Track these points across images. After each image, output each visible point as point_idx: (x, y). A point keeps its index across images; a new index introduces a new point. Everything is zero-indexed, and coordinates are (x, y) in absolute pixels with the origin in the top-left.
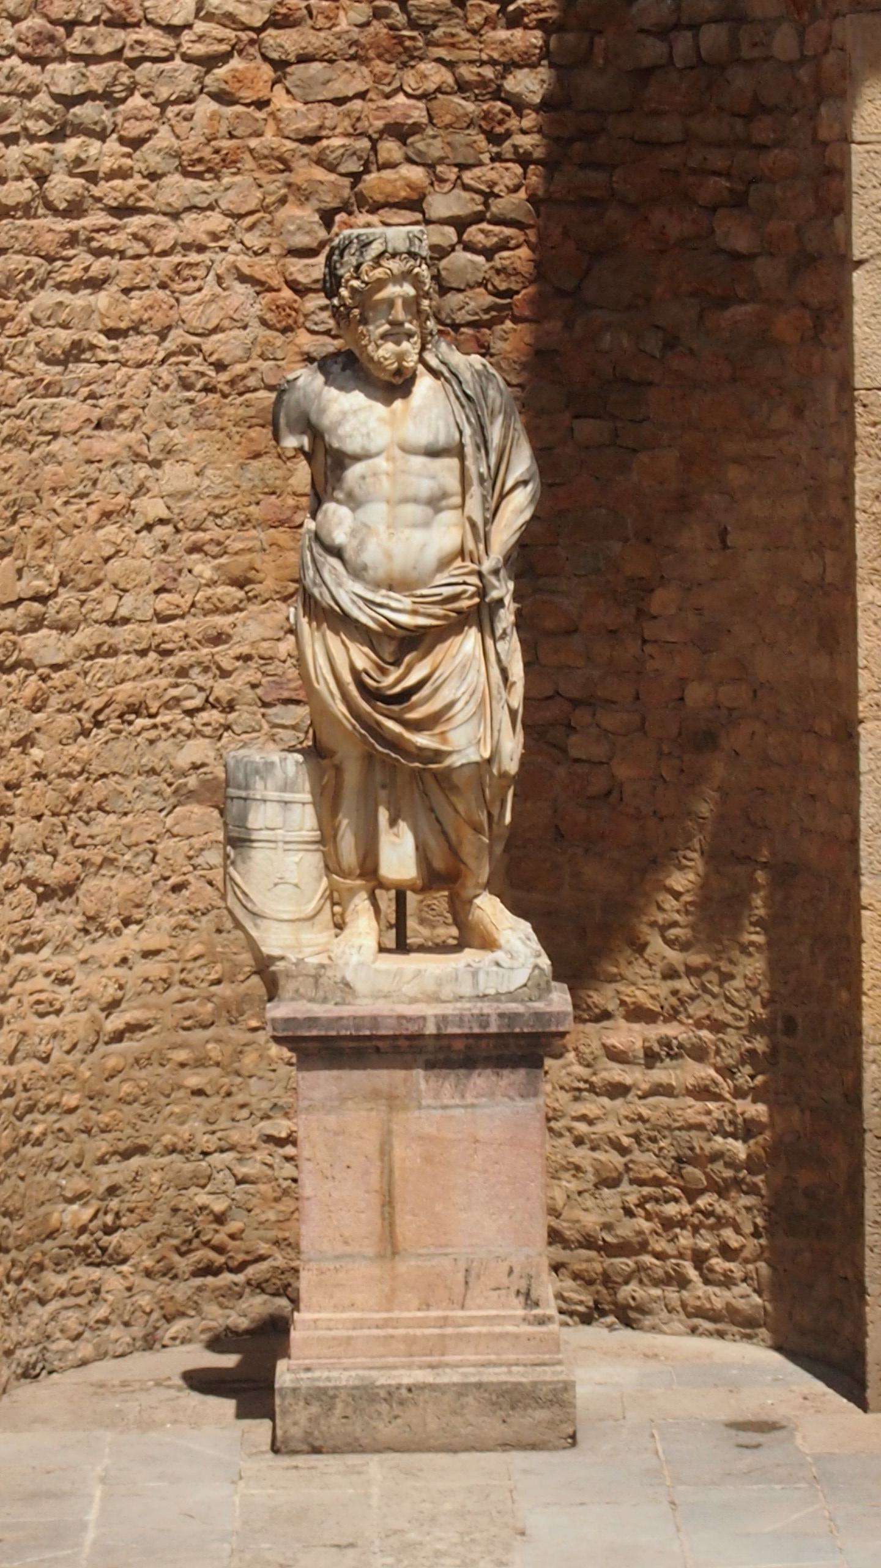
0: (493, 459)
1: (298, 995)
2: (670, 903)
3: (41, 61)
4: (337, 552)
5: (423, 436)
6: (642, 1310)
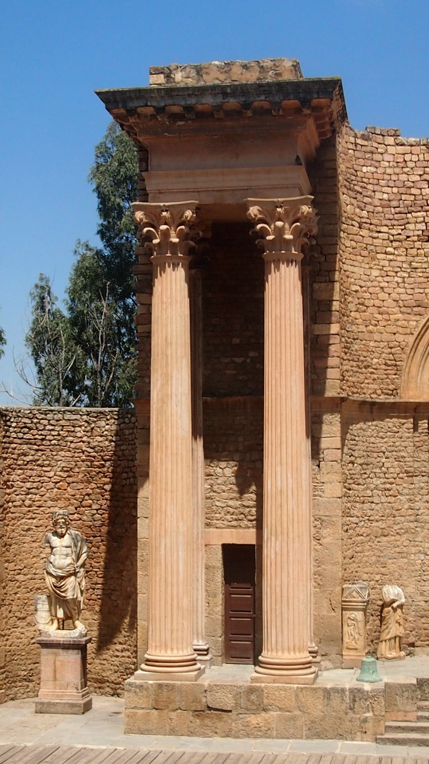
0: (79, 548)
1: (43, 636)
2: (125, 624)
3: (24, 482)
4: (51, 563)
5: (65, 544)
6: (120, 694)
